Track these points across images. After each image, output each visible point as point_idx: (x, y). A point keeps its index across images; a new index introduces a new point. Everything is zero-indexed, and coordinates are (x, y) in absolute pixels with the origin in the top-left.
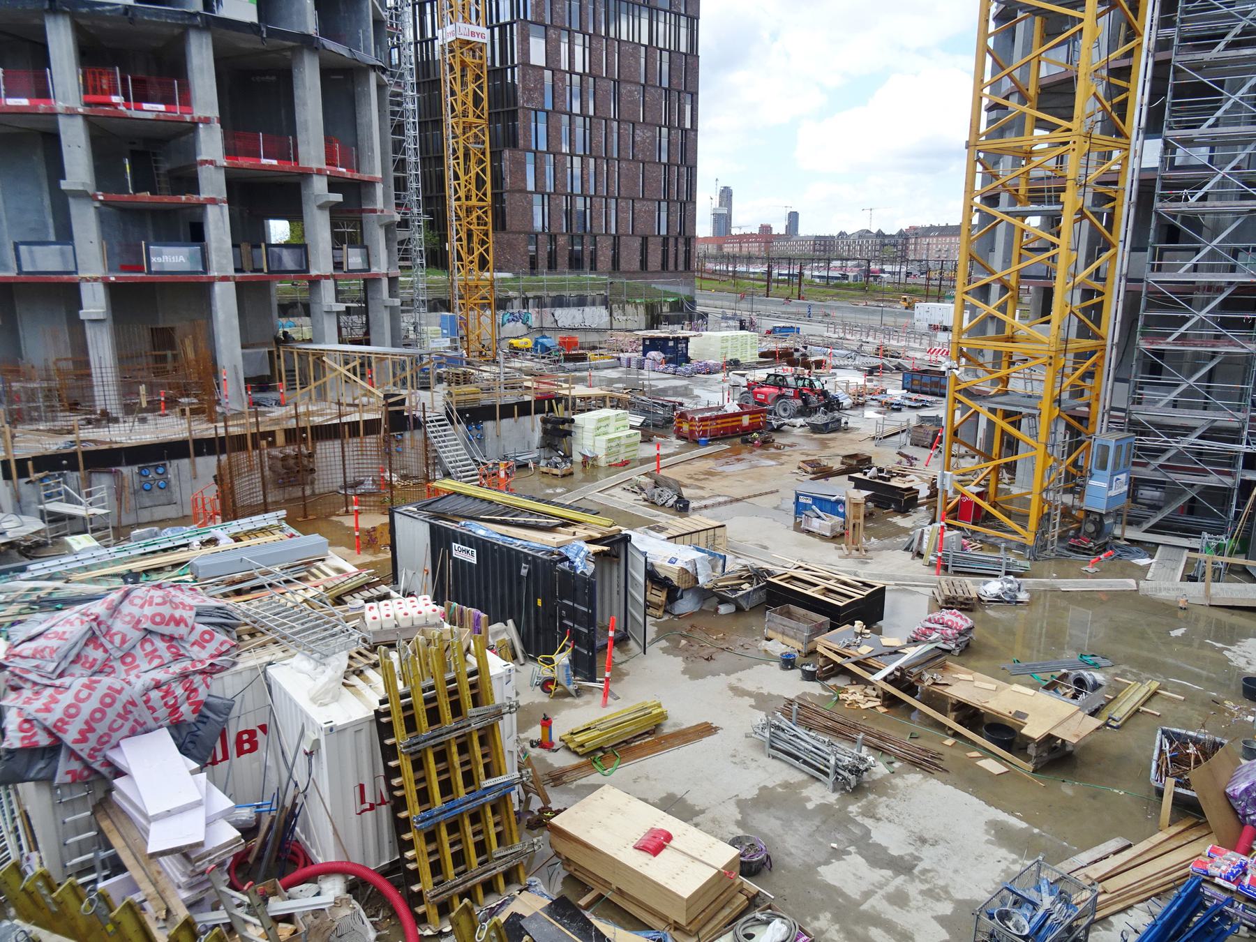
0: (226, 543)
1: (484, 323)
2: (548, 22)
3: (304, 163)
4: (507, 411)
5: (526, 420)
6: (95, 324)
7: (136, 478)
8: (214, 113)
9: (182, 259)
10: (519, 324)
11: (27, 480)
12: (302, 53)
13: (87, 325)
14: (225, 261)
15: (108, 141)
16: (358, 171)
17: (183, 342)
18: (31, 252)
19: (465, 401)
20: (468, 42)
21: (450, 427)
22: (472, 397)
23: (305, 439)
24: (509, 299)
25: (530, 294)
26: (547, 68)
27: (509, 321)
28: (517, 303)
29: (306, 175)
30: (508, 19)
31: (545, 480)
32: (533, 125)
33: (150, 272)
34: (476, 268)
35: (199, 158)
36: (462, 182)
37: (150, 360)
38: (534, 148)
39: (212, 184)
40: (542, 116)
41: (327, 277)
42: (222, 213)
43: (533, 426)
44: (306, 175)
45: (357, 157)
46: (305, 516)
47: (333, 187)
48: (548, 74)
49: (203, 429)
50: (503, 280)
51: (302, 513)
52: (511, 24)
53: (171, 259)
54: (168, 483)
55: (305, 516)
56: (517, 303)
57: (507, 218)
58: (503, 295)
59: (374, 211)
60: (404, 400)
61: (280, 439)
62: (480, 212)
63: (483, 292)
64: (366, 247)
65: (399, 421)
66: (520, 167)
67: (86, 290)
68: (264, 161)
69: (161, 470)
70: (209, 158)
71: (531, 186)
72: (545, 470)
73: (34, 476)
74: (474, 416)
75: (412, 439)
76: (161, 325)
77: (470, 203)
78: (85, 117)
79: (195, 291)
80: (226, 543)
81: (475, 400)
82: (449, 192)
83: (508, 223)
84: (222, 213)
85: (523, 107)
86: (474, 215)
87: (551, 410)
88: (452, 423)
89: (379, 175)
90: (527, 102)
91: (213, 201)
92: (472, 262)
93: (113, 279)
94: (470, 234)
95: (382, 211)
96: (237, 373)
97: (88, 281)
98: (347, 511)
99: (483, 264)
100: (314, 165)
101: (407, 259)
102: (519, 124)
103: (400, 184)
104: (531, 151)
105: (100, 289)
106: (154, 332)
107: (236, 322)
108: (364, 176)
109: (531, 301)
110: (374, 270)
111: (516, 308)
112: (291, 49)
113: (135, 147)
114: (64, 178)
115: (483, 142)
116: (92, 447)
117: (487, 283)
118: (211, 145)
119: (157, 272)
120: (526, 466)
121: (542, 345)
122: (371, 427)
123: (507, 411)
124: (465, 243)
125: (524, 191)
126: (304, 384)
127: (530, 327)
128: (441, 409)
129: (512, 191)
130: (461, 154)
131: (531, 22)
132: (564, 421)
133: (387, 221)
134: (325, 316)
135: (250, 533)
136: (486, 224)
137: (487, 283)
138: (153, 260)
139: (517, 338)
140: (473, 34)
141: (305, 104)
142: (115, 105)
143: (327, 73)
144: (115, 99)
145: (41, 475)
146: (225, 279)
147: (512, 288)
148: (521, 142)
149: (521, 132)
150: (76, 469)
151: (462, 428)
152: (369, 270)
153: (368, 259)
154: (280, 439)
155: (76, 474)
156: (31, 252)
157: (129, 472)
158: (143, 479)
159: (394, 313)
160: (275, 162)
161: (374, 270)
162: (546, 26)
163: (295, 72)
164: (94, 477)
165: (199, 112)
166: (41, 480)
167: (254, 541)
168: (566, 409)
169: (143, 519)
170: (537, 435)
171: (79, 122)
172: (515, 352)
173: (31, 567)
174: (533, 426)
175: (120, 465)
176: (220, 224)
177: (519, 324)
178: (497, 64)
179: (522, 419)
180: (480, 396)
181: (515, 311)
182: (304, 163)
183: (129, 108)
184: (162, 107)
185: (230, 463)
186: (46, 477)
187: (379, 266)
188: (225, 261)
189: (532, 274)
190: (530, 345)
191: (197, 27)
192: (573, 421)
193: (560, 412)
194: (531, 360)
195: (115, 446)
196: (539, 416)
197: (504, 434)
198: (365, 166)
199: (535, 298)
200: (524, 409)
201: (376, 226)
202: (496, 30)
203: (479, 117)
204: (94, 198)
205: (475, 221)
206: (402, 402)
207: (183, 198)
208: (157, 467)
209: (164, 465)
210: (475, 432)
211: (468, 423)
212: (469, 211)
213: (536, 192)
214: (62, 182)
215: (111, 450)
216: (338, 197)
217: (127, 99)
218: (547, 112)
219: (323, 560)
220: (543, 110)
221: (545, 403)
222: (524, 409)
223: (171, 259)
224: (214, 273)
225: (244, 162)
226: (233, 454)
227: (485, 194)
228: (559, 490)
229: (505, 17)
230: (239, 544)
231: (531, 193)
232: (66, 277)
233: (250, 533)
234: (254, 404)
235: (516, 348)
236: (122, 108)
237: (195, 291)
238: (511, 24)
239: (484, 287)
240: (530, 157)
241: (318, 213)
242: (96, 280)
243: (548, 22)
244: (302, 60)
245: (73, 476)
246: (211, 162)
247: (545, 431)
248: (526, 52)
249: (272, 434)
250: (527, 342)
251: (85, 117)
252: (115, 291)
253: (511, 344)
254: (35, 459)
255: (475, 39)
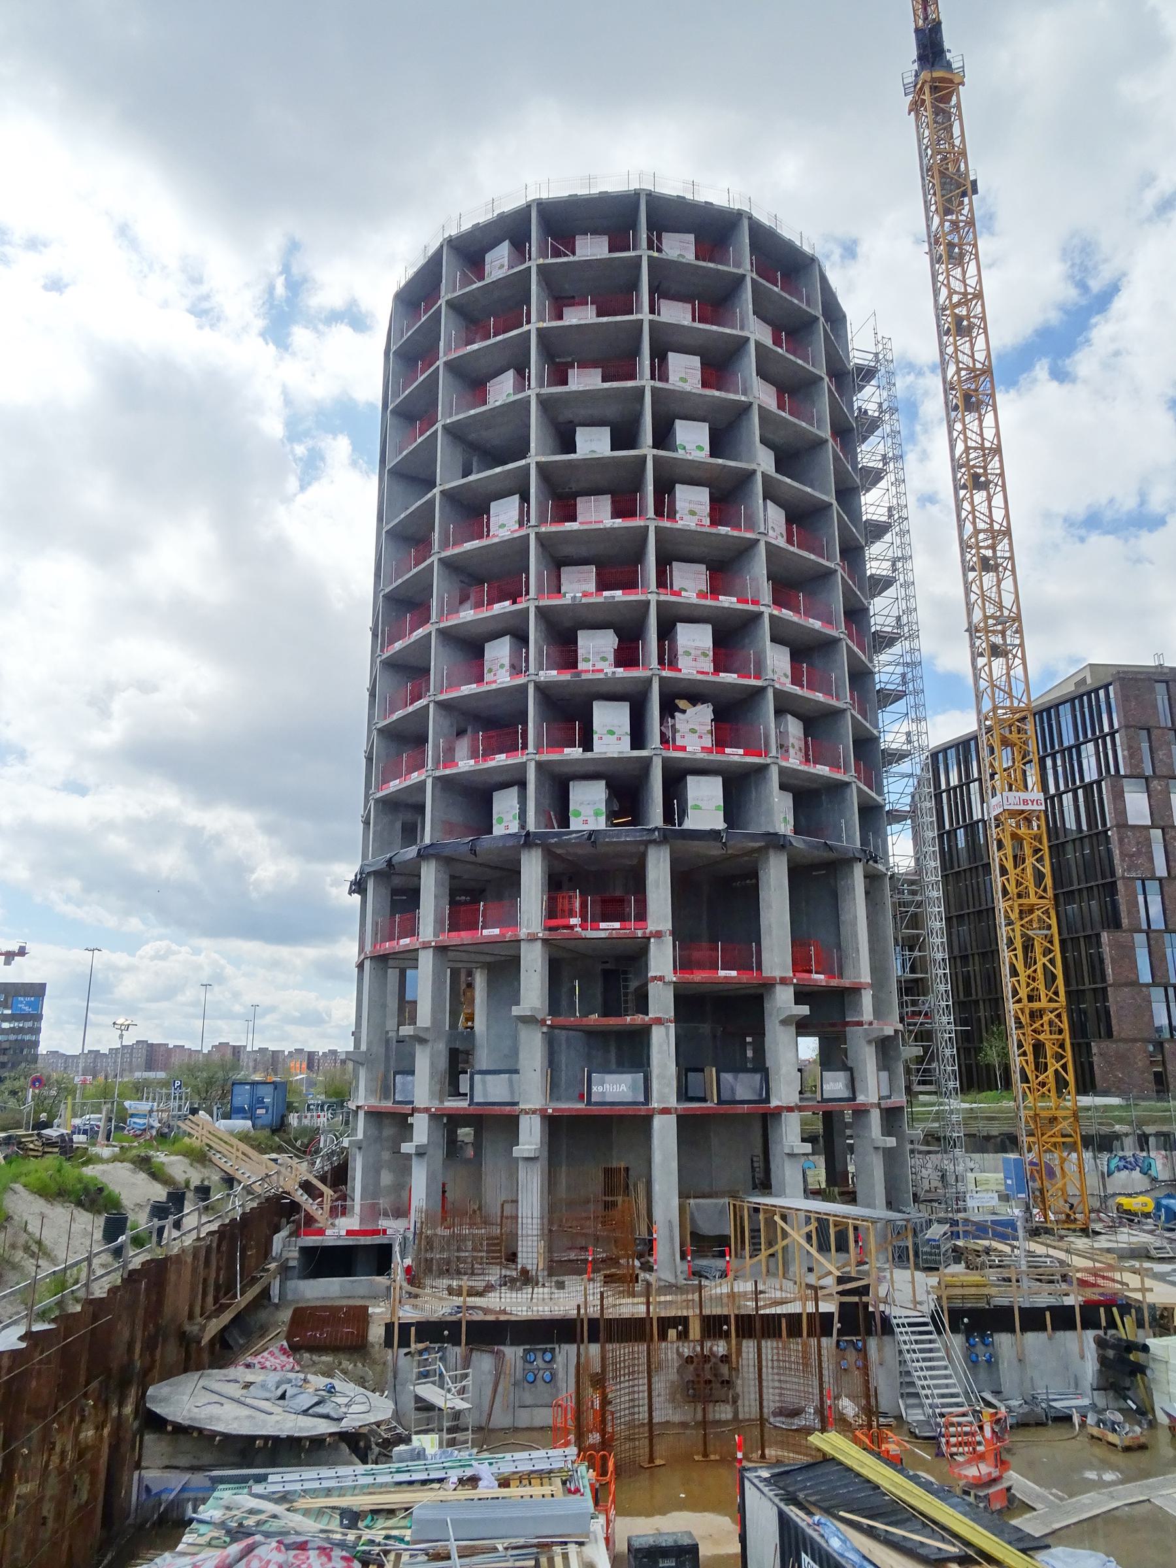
0: (488, 1488)
1: (1080, 1172)
2: (1149, 772)
3: (768, 972)
4: (1033, 1320)
5: (1068, 1339)
6: (531, 1163)
7: (520, 1363)
8: (667, 925)
9: (624, 1087)
10: (1136, 1174)
11: (406, 1350)
12: (767, 853)
13: (521, 1163)
14: (667, 1090)
15: (563, 963)
16: (841, 976)
17: (635, 1185)
18: (484, 1082)
19: (963, 1297)
20: (1023, 812)
21: (934, 1336)
22: (973, 1291)
23: (727, 1335)
24: (1117, 1136)
25: (1150, 1129)
26: (1153, 827)
27: (1119, 1169)
28: (1129, 1142)
29: (768, 986)
30: (1095, 777)
31: (1099, 1451)
32: (1141, 899)
33: (589, 1103)
34: (1053, 1094)
35: (650, 975)
36: (1023, 977)
37: (601, 1207)
38: (1144, 926)
39: (661, 1002)
40: (1153, 886)
41: (790, 1109)
42: (667, 1035)
43: (1081, 1350)
44: (768, 986)
45: (840, 959)
46: (705, 1455)
47: (799, 998)
48: (1156, 834)
49: (630, 1307)
50: (1107, 1108)
51: (701, 1448)
52: (1099, 782)
53: (614, 1088)
54: (553, 1375)
55: (705, 1455)
56: (1129, 1142)
57: (1114, 1022)
58: (1105, 1130)
59: (860, 1024)
60: (867, 1287)
61: (695, 1330)
62: (1052, 1016)
63: (1064, 1126)
64: (851, 1070)
65: (859, 1320)
66: (1127, 954)
67: (524, 1121)
68: (722, 973)
69: (548, 1357)
70: (658, 974)
71: (1145, 977)
72: (1095, 1431)
73: (414, 1346)
74: (977, 1321)
75: (880, 1350)
76: (614, 1165)
77: (1036, 1005)
78: (545, 941)
79: (633, 1124)
80: (488, 1488)
81: (979, 1297)
82: (1008, 991)
83: (1115, 1028)
84: (667, 1035)
85: (1123, 878)
86: (1045, 1018)
87: (1112, 1324)
88: (939, 1333)
89: (866, 977)
90: (1129, 870)
91: (659, 1021)
92: (1043, 1084)
93: (550, 1111)
94: (1038, 1048)
95: (871, 1024)
96: (671, 1231)
97: (527, 1113)
98: (763, 1456)
99: (1061, 1084)
100: (777, 974)
101: (930, 1083)
102: (1121, 898)
103: (913, 988)
104: (1141, 931)
105: (536, 1120)
106: (609, 1173)
107: (674, 1165)
108: (846, 982)
109: (1152, 1140)
110: (861, 1098)
111: (1129, 1149)
112: (759, 850)
113: (608, 966)
114: (518, 1003)
115: (1049, 927)
116: (478, 1316)
117: (1068, 1113)
118: (661, 961)
119: (597, 1104)
120: (1069, 1418)
121: (1168, 1208)
122: (822, 1325)
123: (1033, 1320)
124: (1030, 1057)
125: (1135, 984)
126: (755, 1251)
127: (1154, 1179)
128: (929, 1306)
129: (1118, 985)
130: (1018, 943)
131: (1125, 777)
132: (1131, 1347)
133: (875, 1035)
134: (786, 1158)
135: (526, 1478)
136: (1061, 1031)
137: (1068, 1113)
138: (594, 1089)
139: (1130, 1195)
140: (1025, 802)
141: (770, 907)
142: (572, 927)
143: (799, 874)
144: (574, 921)
145: (421, 1346)
146: (665, 1111)
147: (1121, 1121)
148: (1125, 922)
149: (1123, 909)
150: (458, 1343)
151: (957, 1341)
152: (854, 1099)
153: (852, 1085)
154: (695, 1330)
155: (457, 1349)
156: (484, 1082)
157: (513, 1353)
158: (528, 1366)
159: (890, 1156)
160: (734, 973)
161: (861, 1098)
162: (1147, 778)
163: (761, 873)
164: (476, 1356)
165: (652, 926)
166: (421, 1353)
167: (526, 1491)
168: (1140, 1324)
169: (522, 1423)
170: (1090, 1368)
171: (539, 944)
172: (1130, 1218)
173: (271, 1478)
174: (1081, 1350)
175: (504, 1344)
176: (665, 1047)
177: (1136, 1174)
178: (1085, 827)
179: (1060, 1335)
180: (993, 1291)
181: (1128, 1153)
182: (768, 972)
183: (584, 928)
184: (617, 925)
185: (603, 1359)
186: (426, 1349)
187: (866, 1092)
188: (667, 1090)
189: (1160, 1099)
190: (1151, 1207)
191: (654, 842)
192: (1145, 1348)
193: (1127, 1330)
194: (1151, 1232)
195: (503, 1318)
196: (1090, 1334)
197: (1032, 1357)
198: (849, 972)
199: (1158, 1135)
200: (1063, 1319)
201: (863, 1042)
202: (1080, 792)
203: (1042, 897)
204: (543, 1022)
205: (1046, 1027)
206: (865, 1291)
207: (628, 1018)
208: (545, 1351)
209: (552, 1350)
210: (980, 1349)
211: (968, 1335)
212: (1035, 1015)
213: (1154, 984)
214: (514, 1008)
215: (497, 1323)
216: (805, 1010)
217: (584, 918)
218: (1160, 880)
219: (581, 1544)
220: (1153, 878)
221: (1099, 1313)
222: (1063, 1319)
223: (614, 1088)
224: (655, 1105)
225: (698, 976)
226: (609, 1346)
227: (1056, 993)
228: (1109, 1476)
229: (1091, 774)
230: (505, 1492)
231: (1148, 985)
232: (508, 1108)
233: (526, 1478)
234: (694, 1274)
235: (1128, 1212)
236: (578, 929)
237: (633, 1124)
238: (1099, 782)
239: (1065, 1118)
240: (1140, 939)
241: (780, 1029)
242: (534, 1112)
243: (1149, 772)
244: (768, 858)
245: (456, 1352)
246: (661, 978)
247: (1103, 1361)
248: (1121, 812)
249: (684, 1321)
250: (1143, 1203)
251: (545, 941)
252: (554, 1125)
253: (1120, 1205)
254: (419, 1324)
255: (1029, 807)
